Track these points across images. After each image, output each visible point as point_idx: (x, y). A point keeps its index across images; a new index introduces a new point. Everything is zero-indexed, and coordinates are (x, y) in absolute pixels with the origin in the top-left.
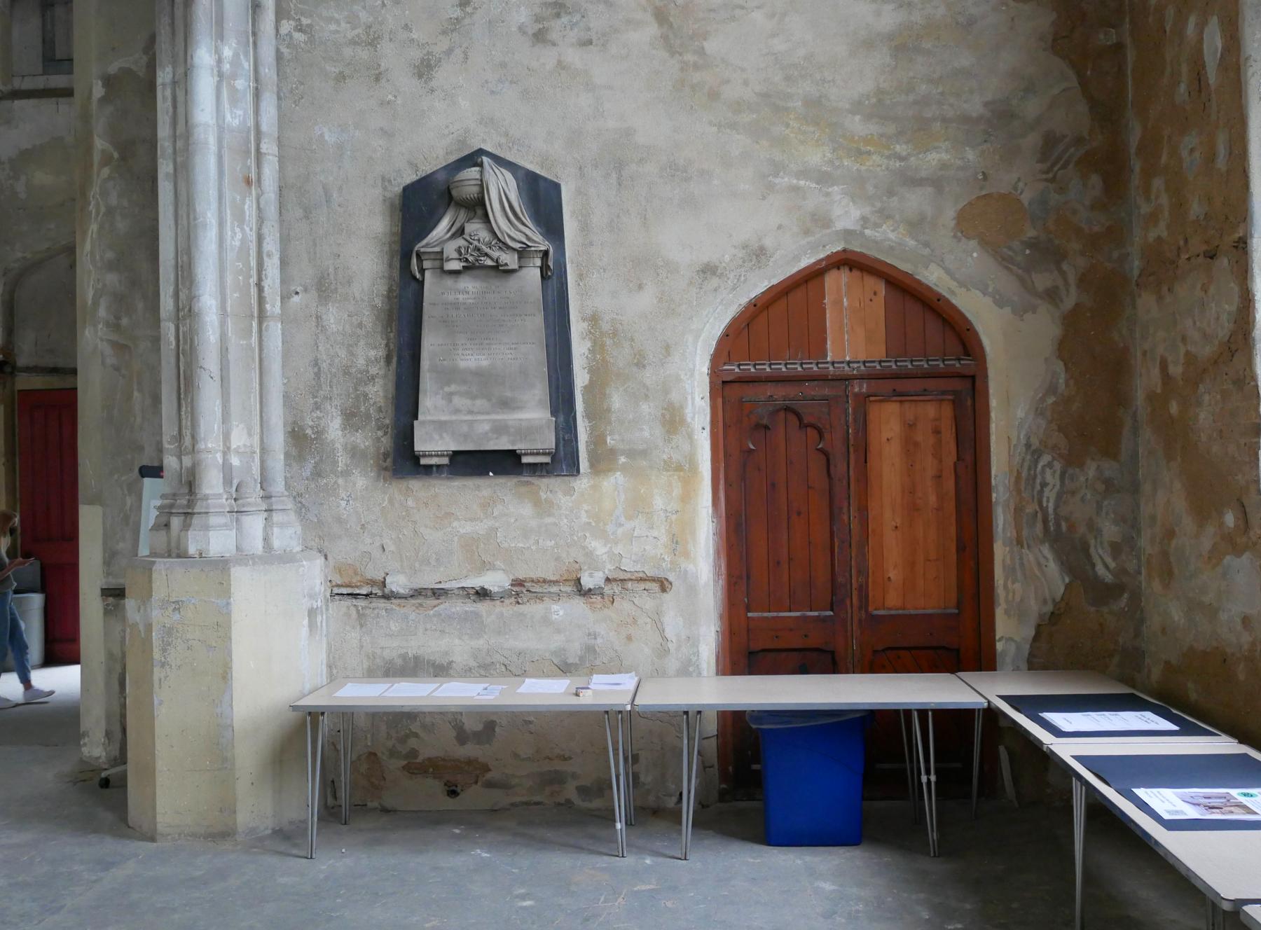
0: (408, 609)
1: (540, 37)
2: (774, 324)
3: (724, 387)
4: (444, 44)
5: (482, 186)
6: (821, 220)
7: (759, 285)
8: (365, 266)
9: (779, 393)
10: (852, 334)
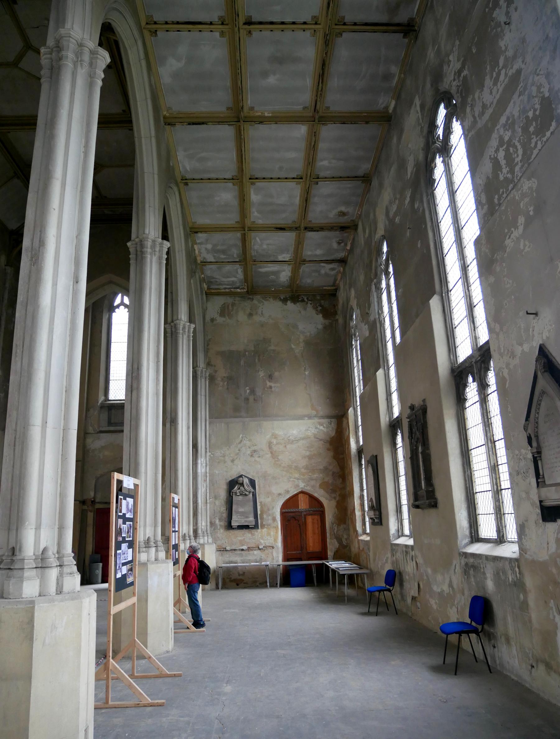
0: (230, 553)
1: (252, 456)
2: (290, 503)
3: (282, 514)
4: (236, 457)
5: (243, 481)
6: (298, 486)
7: (288, 497)
8: (223, 494)
9: (292, 514)
10: (303, 505)
